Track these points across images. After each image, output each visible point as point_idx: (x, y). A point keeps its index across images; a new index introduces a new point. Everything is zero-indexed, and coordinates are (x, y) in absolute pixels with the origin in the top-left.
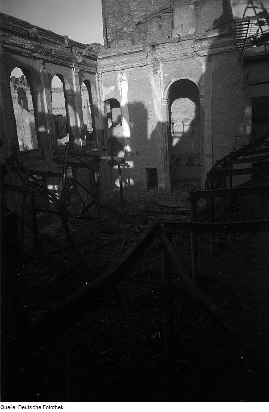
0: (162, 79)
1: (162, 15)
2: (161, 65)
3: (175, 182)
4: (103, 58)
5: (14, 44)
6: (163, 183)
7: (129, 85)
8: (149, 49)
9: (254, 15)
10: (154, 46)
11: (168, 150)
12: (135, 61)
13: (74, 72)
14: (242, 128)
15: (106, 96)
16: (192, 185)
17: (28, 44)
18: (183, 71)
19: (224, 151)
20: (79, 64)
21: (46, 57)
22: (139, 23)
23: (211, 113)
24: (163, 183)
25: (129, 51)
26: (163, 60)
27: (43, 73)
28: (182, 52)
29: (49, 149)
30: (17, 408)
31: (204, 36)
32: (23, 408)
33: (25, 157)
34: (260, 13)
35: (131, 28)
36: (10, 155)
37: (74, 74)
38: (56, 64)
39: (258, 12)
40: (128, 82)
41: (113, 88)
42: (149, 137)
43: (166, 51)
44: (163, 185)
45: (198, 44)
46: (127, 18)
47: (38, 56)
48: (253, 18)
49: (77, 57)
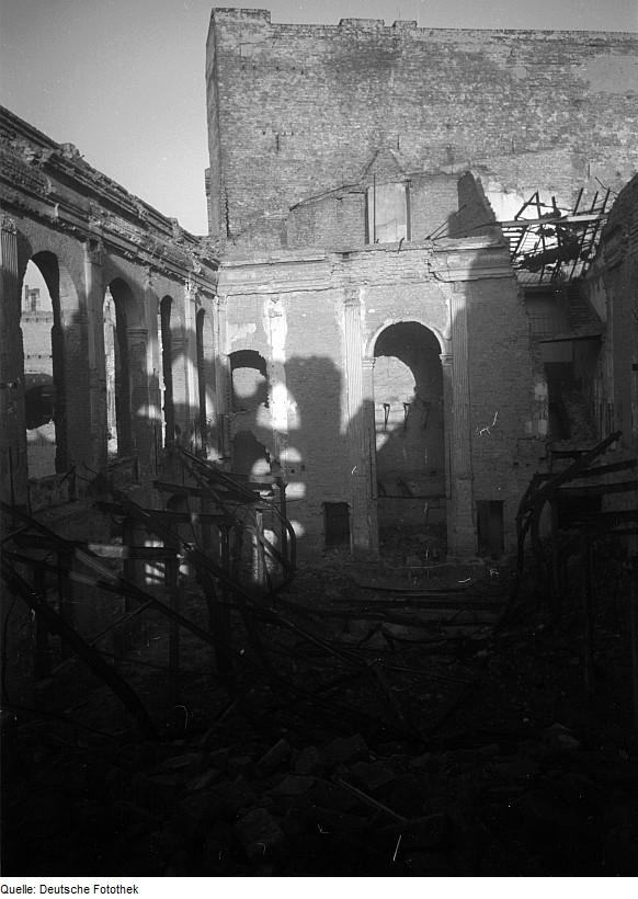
0: (363, 318)
1: (344, 196)
2: (362, 292)
3: (388, 534)
4: (233, 267)
5: (115, 234)
6: (363, 535)
7: (290, 325)
8: (335, 259)
9: (537, 217)
10: (346, 254)
12: (307, 278)
14: (530, 424)
15: (232, 345)
16: (417, 539)
17: (134, 233)
18: (407, 307)
19: (495, 469)
21: (154, 261)
22: (295, 207)
24: (363, 535)
25: (295, 259)
26: (366, 281)
28: (406, 271)
30: (37, 890)
31: (453, 246)
32: (50, 890)
35: (281, 214)
36: (97, 471)
37: (188, 297)
39: (543, 214)
40: (288, 318)
41: (252, 328)
42: (343, 429)
43: (373, 265)
44: (362, 540)
45: (439, 259)
46: (272, 193)
48: (534, 221)
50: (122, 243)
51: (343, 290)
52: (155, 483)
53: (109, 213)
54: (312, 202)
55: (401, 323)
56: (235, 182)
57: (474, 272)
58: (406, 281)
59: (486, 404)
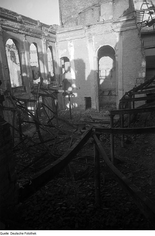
0: (94, 45)
1: (94, 8)
2: (93, 37)
3: (101, 105)
4: (60, 33)
5: (8, 26)
6: (95, 105)
7: (75, 49)
8: (86, 28)
9: (147, 8)
10: (89, 26)
11: (97, 86)
13: (43, 41)
15: (61, 55)
17: (16, 25)
20: (46, 36)
21: (26, 33)
23: (122, 65)
24: (95, 105)
25: (75, 29)
26: (94, 34)
27: (25, 42)
28: (105, 30)
29: (28, 86)
30: (10, 234)
32: (13, 234)
33: (15, 91)
34: (150, 7)
35: (76, 16)
37: (43, 43)
38: (33, 37)
39: (149, 7)
41: (65, 50)
42: (86, 79)
46: (73, 10)
47: (22, 32)
48: (147, 10)
49: (45, 33)
50: (11, 28)
51: (88, 37)
52: (32, 92)
53: (4, 20)
54: (85, 11)
55: (104, 46)
56: (63, 8)
57: (122, 28)
58: (105, 33)
59: (128, 69)
